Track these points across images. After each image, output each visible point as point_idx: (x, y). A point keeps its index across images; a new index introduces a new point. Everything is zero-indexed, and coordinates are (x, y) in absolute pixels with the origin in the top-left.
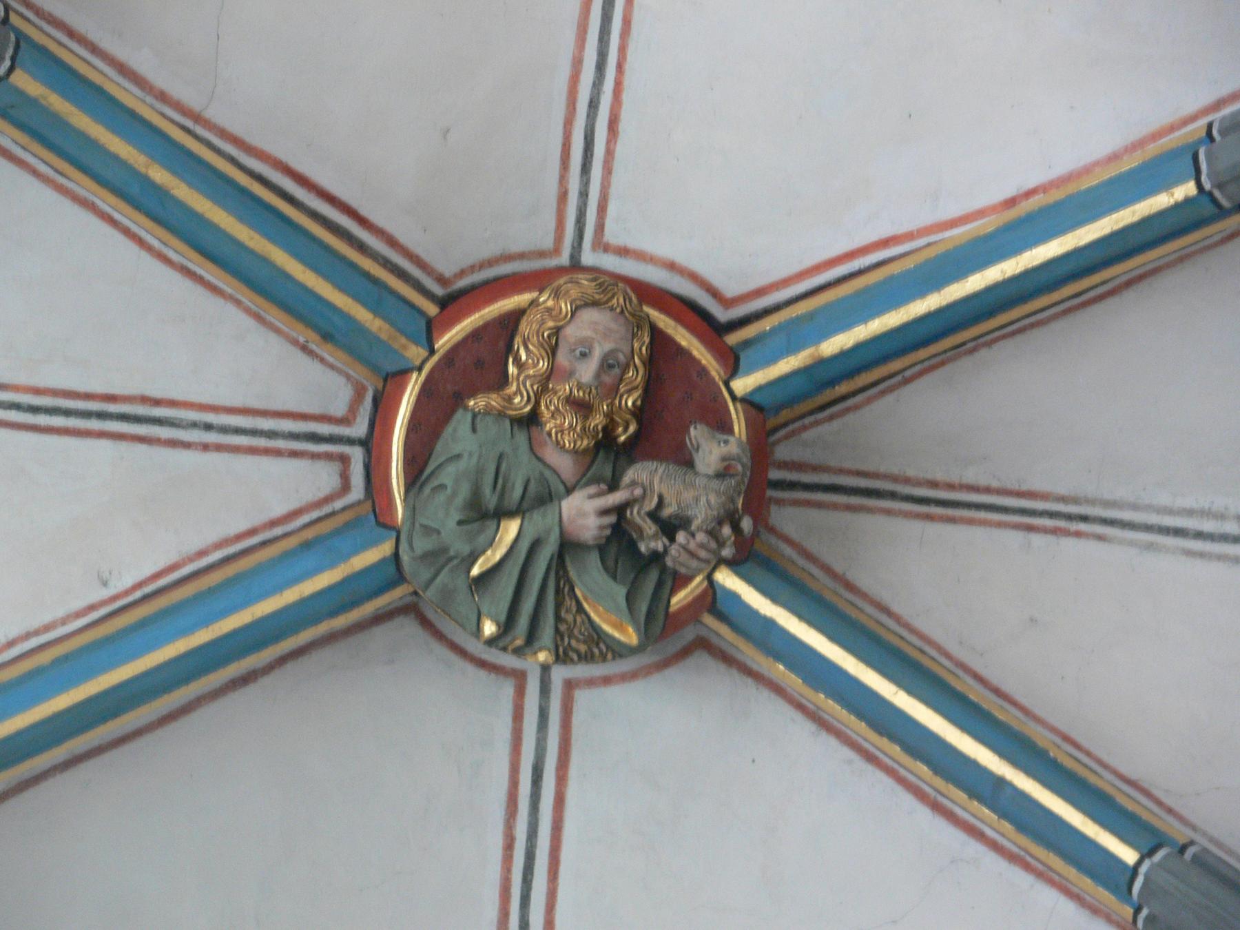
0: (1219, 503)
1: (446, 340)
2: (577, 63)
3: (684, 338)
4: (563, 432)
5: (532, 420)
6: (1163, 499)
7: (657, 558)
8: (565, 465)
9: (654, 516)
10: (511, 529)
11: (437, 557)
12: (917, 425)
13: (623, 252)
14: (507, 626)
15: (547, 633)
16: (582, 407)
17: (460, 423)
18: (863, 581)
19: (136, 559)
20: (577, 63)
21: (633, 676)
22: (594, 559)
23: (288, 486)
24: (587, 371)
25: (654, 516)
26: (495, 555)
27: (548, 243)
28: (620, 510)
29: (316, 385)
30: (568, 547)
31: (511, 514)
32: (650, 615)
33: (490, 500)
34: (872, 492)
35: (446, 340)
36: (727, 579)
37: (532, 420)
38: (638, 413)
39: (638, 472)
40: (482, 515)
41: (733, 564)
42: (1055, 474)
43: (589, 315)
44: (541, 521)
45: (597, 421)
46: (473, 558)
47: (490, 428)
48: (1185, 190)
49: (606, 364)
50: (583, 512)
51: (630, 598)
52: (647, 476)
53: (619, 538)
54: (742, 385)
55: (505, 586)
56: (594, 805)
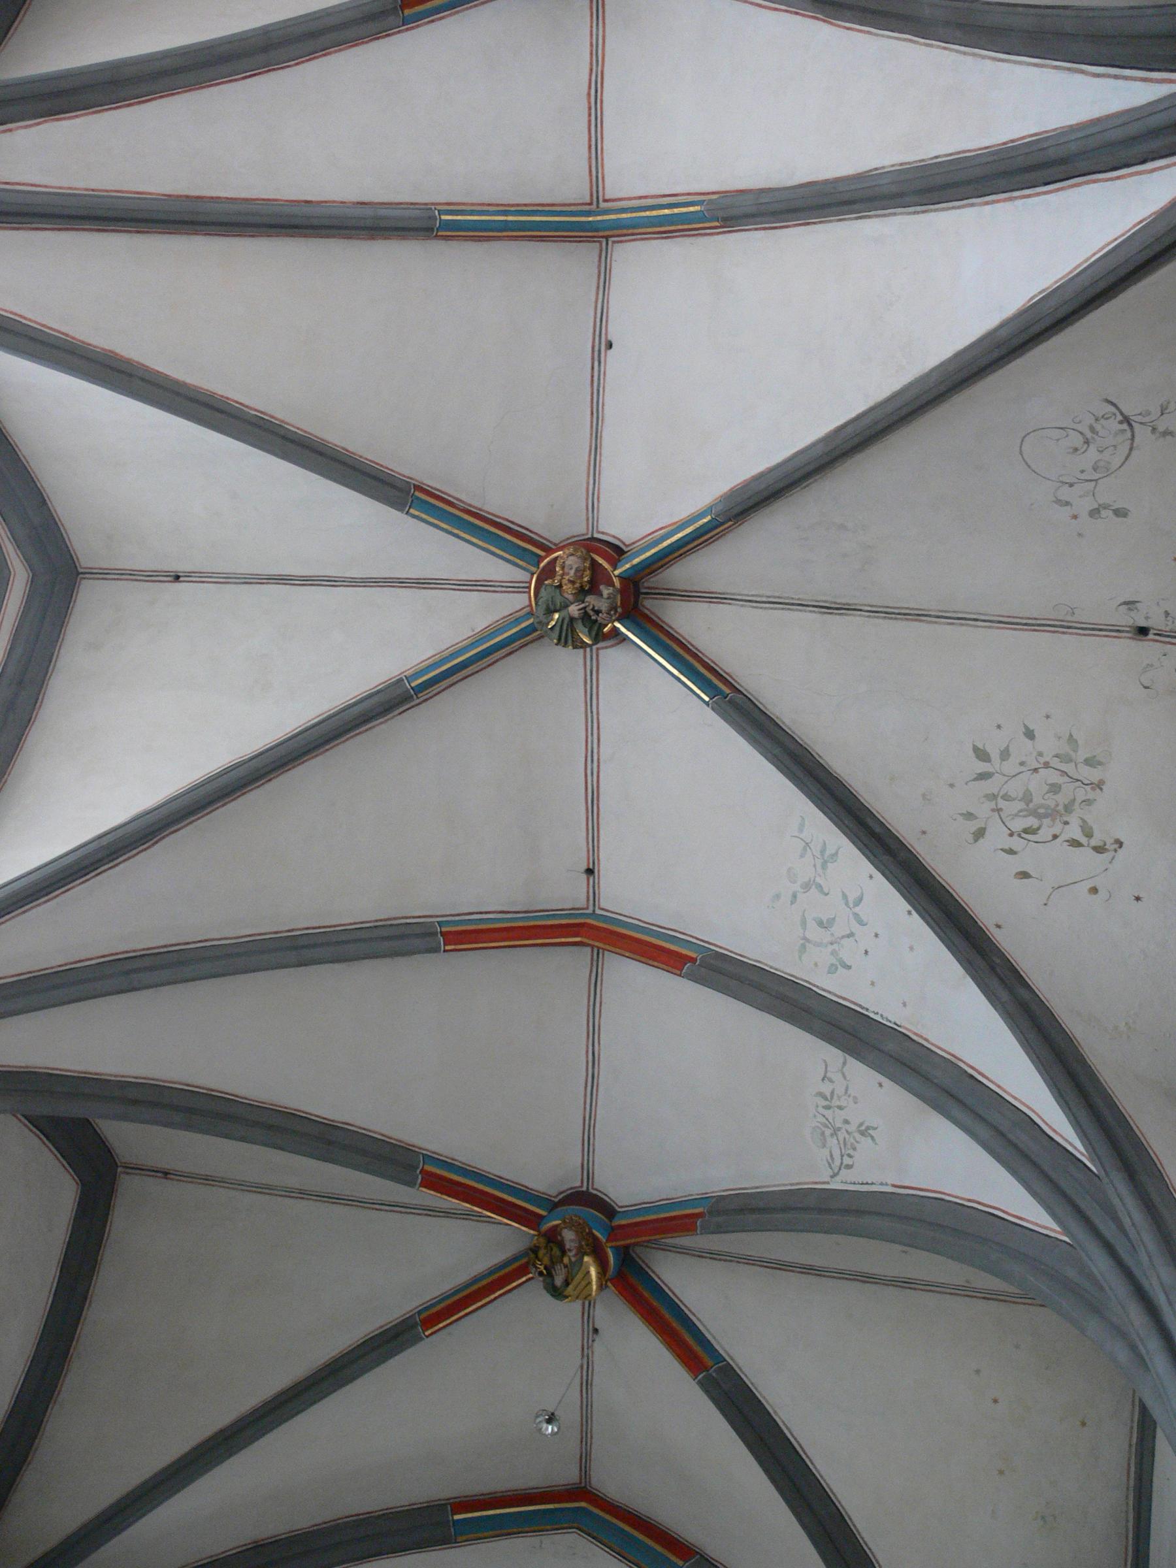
0: (761, 592)
1: (542, 565)
2: (588, 483)
3: (601, 561)
4: (569, 591)
5: (560, 586)
6: (746, 592)
7: (596, 621)
8: (570, 597)
9: (593, 609)
10: (556, 616)
11: (540, 623)
12: (679, 574)
13: (603, 533)
14: (559, 639)
15: (570, 641)
16: (572, 582)
17: (543, 590)
18: (667, 620)
19: (482, 623)
20: (588, 483)
21: (612, 646)
22: (580, 622)
23: (519, 602)
24: (572, 572)
25: (593, 609)
26: (553, 623)
27: (584, 531)
28: (584, 608)
29: (520, 575)
30: (572, 619)
31: (556, 611)
32: (597, 635)
33: (552, 608)
34: (670, 594)
35: (542, 565)
36: (617, 625)
37: (560, 586)
38: (589, 582)
39: (588, 599)
40: (550, 612)
41: (618, 620)
42: (718, 587)
43: (572, 558)
44: (564, 613)
45: (578, 585)
46: (548, 624)
47: (549, 589)
48: (709, 518)
49: (577, 570)
50: (574, 610)
51: (590, 632)
52: (591, 600)
53: (585, 617)
54: (617, 572)
55: (557, 629)
56: (607, 680)
